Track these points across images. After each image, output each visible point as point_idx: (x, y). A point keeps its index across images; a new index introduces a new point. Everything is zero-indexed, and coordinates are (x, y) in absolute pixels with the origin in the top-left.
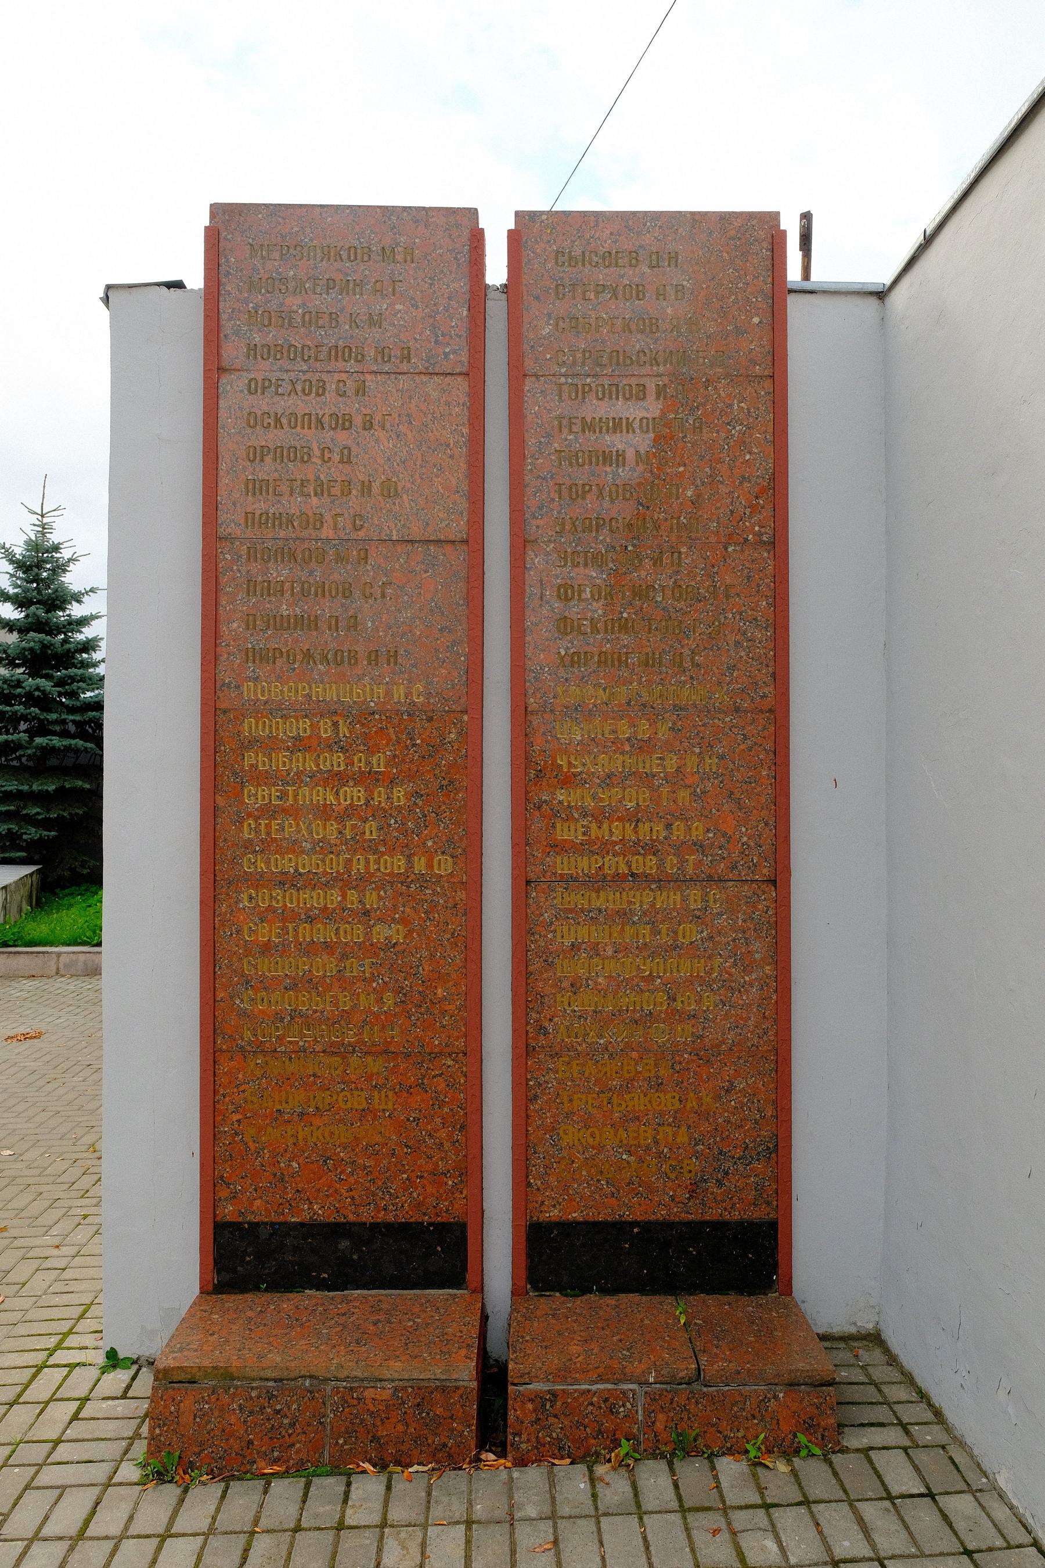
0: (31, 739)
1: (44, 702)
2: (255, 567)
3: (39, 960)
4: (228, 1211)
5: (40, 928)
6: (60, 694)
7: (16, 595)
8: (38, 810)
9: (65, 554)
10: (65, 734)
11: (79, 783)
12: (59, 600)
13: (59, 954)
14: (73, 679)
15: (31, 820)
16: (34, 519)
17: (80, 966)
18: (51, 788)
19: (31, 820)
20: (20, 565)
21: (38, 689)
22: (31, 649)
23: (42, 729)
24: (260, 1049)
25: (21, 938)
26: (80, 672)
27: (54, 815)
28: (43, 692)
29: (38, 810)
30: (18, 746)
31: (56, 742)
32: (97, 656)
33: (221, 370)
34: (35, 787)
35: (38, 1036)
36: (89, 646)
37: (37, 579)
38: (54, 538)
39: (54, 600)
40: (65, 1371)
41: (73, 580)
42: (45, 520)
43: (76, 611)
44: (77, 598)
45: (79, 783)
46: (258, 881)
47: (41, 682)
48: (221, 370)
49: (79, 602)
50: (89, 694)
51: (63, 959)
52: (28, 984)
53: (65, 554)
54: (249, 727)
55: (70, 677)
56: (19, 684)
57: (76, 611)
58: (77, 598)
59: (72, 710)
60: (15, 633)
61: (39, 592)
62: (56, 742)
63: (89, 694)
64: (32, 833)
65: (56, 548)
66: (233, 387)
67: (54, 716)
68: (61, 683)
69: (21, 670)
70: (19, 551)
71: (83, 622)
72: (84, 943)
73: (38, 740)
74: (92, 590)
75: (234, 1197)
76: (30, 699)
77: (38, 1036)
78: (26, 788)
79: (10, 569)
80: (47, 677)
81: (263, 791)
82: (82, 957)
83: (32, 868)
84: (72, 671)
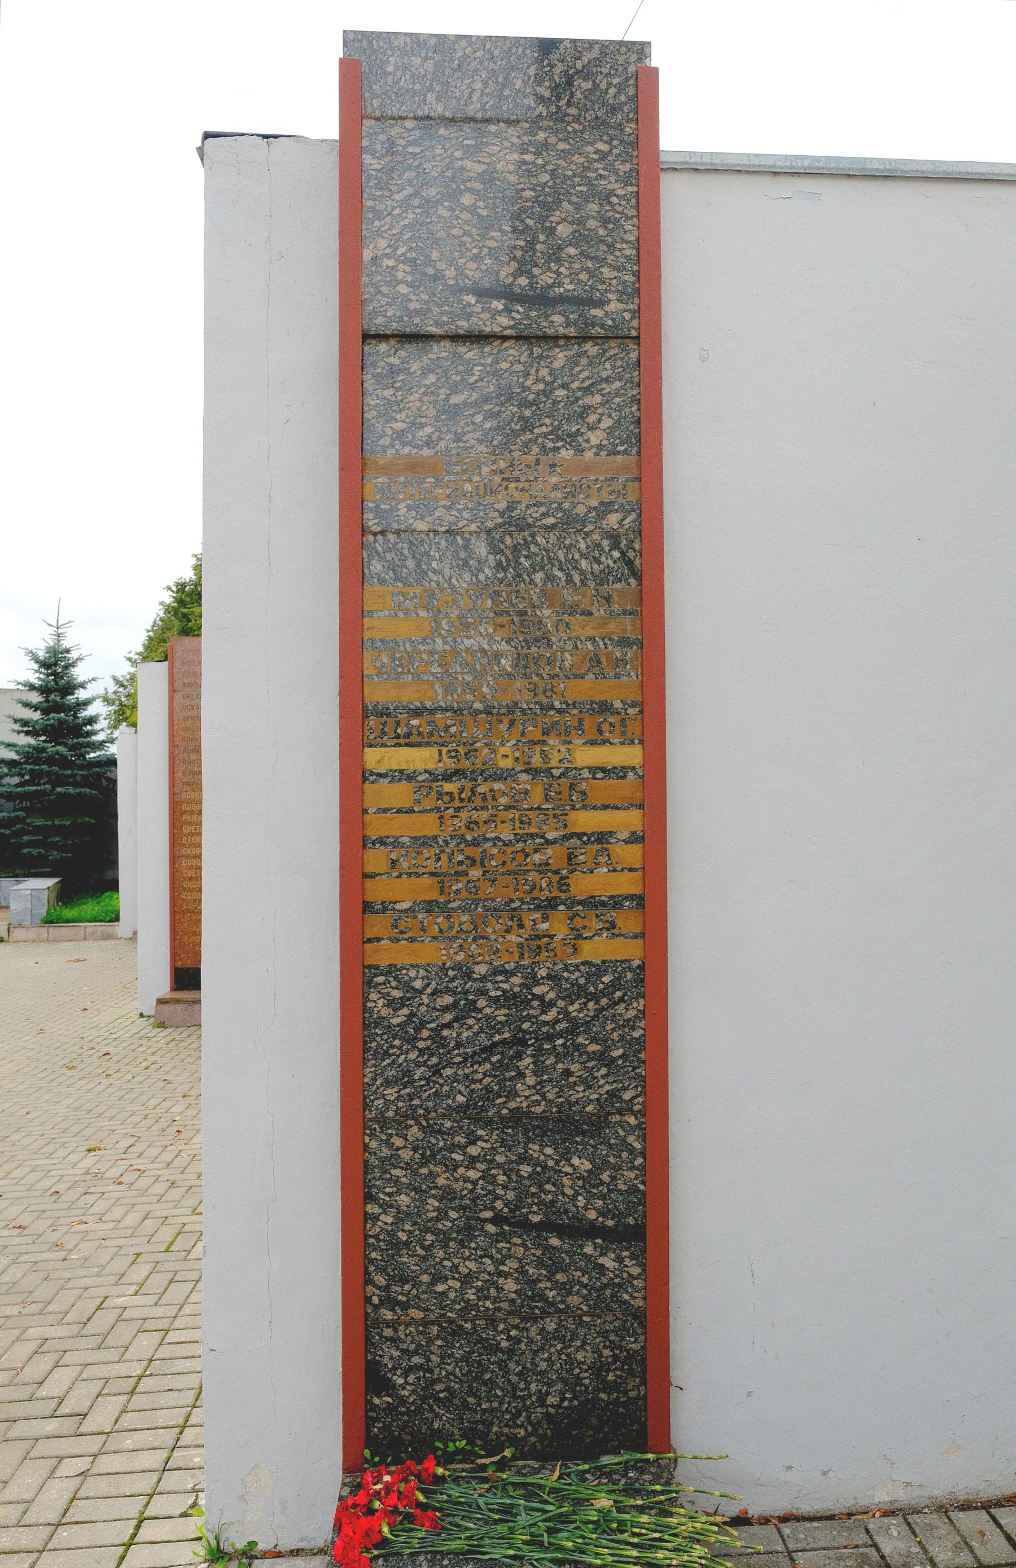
0: (53, 788)
1: (63, 762)
2: (186, 755)
3: (74, 931)
4: (179, 964)
5: (69, 913)
6: (72, 756)
7: (41, 686)
8: (58, 838)
9: (74, 655)
10: (76, 784)
11: (87, 819)
12: (70, 688)
13: (86, 927)
14: (82, 745)
15: (54, 846)
16: (52, 630)
17: (99, 934)
18: (68, 823)
19: (54, 846)
20: (45, 665)
21: (57, 753)
22: (52, 725)
23: (60, 781)
24: (189, 911)
25: (60, 918)
26: (85, 740)
27: (69, 842)
28: (61, 755)
29: (58, 838)
30: (44, 793)
31: (71, 790)
32: (97, 727)
33: (174, 691)
34: (56, 822)
35: (84, 960)
36: (91, 720)
37: (55, 674)
38: (66, 643)
39: (67, 689)
40: (32, 1442)
41: (80, 673)
42: (60, 631)
43: (82, 694)
44: (82, 686)
45: (87, 819)
46: (188, 857)
47: (60, 749)
48: (174, 691)
49: (84, 688)
50: (92, 755)
51: (89, 930)
52: (69, 944)
53: (74, 655)
54: (184, 807)
55: (79, 744)
56: (44, 750)
57: (82, 694)
58: (82, 686)
59: (81, 767)
60: (39, 712)
61: (57, 683)
62: (71, 790)
63: (92, 755)
64: (55, 855)
65: (68, 651)
66: (178, 697)
67: (69, 772)
68: (72, 748)
69: (43, 738)
70: (42, 655)
71: (86, 703)
72: (101, 921)
73: (59, 789)
74: (94, 679)
75: (181, 959)
76: (51, 760)
77: (84, 960)
78: (49, 823)
79: (36, 666)
80: (65, 745)
81: (189, 828)
82: (100, 928)
83: (57, 880)
84: (81, 740)
